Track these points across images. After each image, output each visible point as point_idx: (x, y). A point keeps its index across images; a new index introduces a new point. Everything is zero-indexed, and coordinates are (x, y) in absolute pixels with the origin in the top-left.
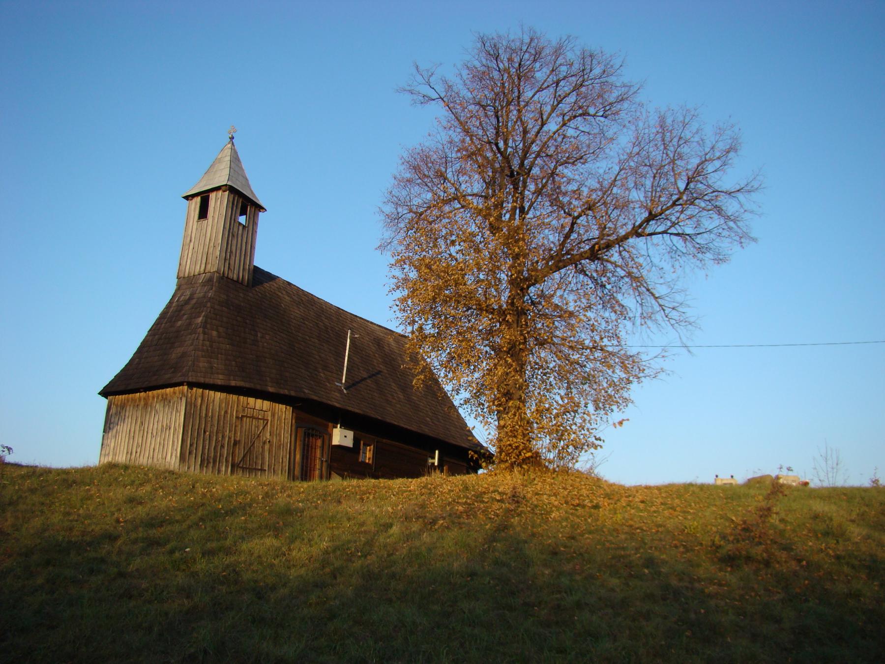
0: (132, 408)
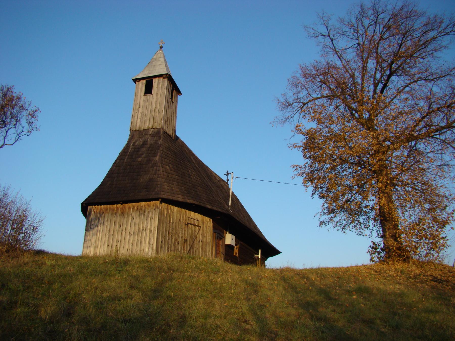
0: (110, 215)
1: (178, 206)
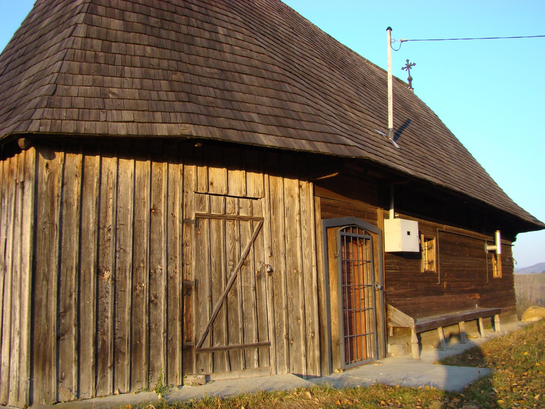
1: (176, 160)
